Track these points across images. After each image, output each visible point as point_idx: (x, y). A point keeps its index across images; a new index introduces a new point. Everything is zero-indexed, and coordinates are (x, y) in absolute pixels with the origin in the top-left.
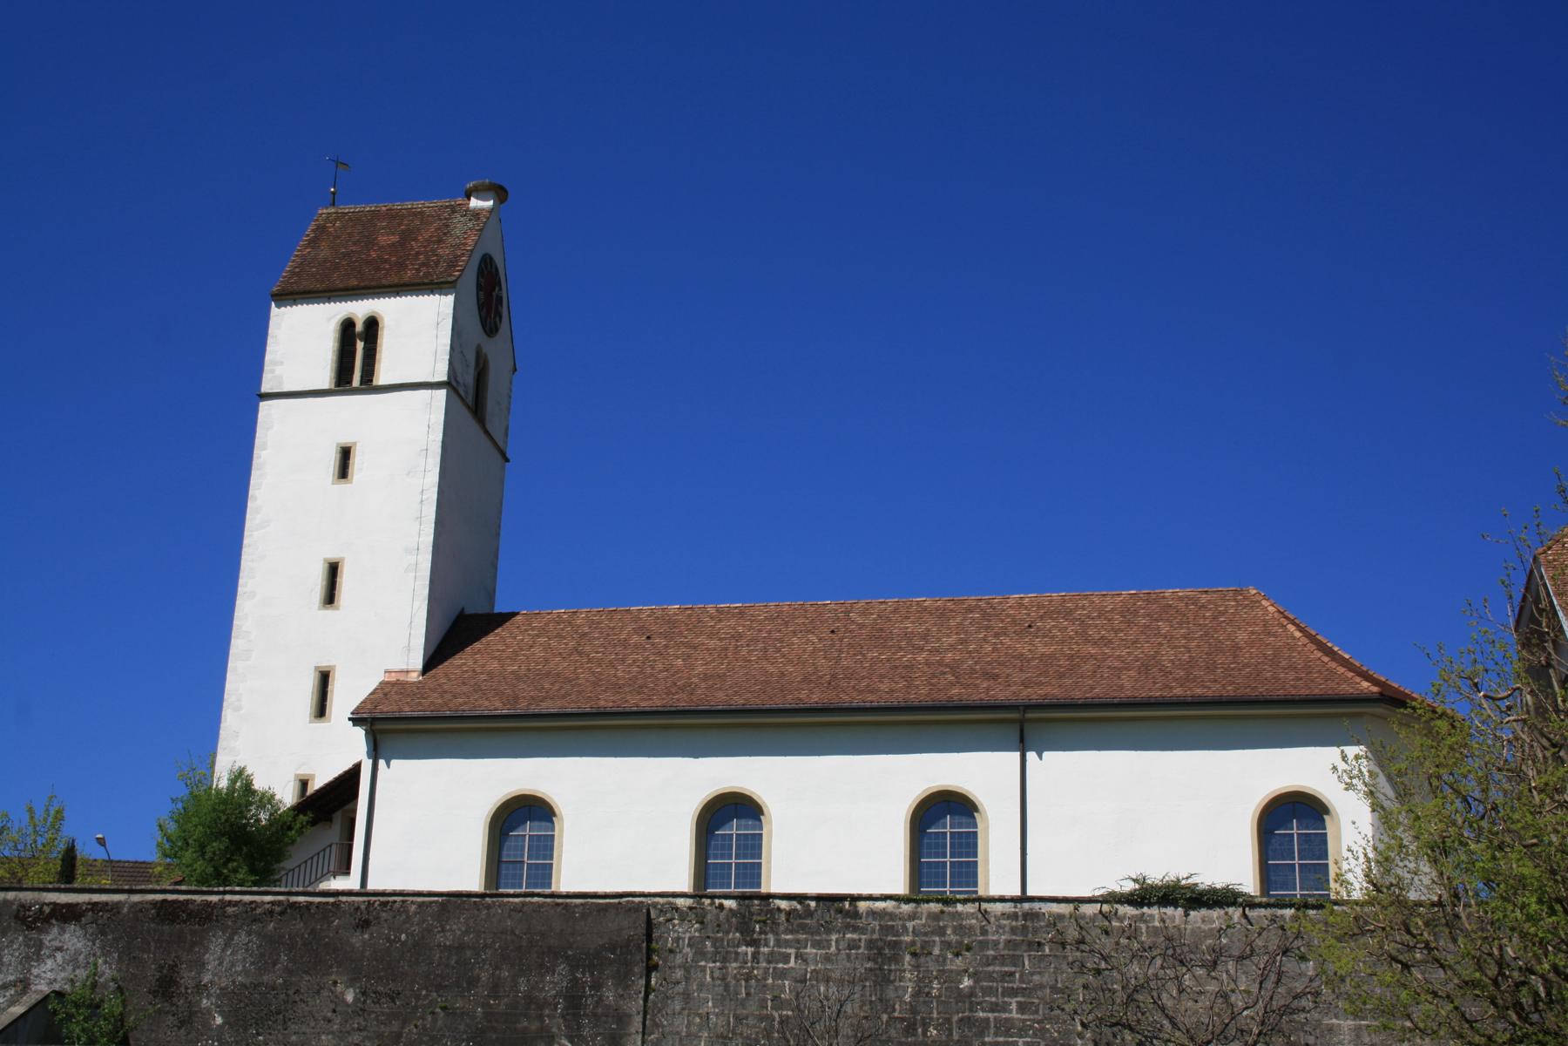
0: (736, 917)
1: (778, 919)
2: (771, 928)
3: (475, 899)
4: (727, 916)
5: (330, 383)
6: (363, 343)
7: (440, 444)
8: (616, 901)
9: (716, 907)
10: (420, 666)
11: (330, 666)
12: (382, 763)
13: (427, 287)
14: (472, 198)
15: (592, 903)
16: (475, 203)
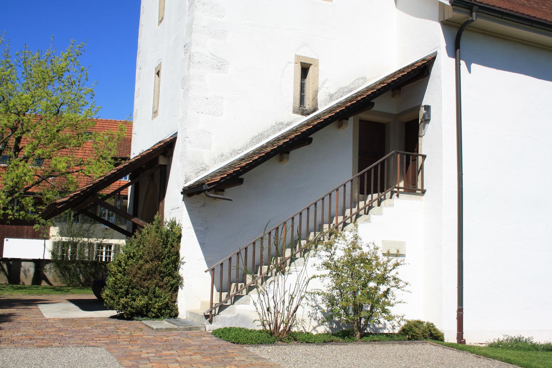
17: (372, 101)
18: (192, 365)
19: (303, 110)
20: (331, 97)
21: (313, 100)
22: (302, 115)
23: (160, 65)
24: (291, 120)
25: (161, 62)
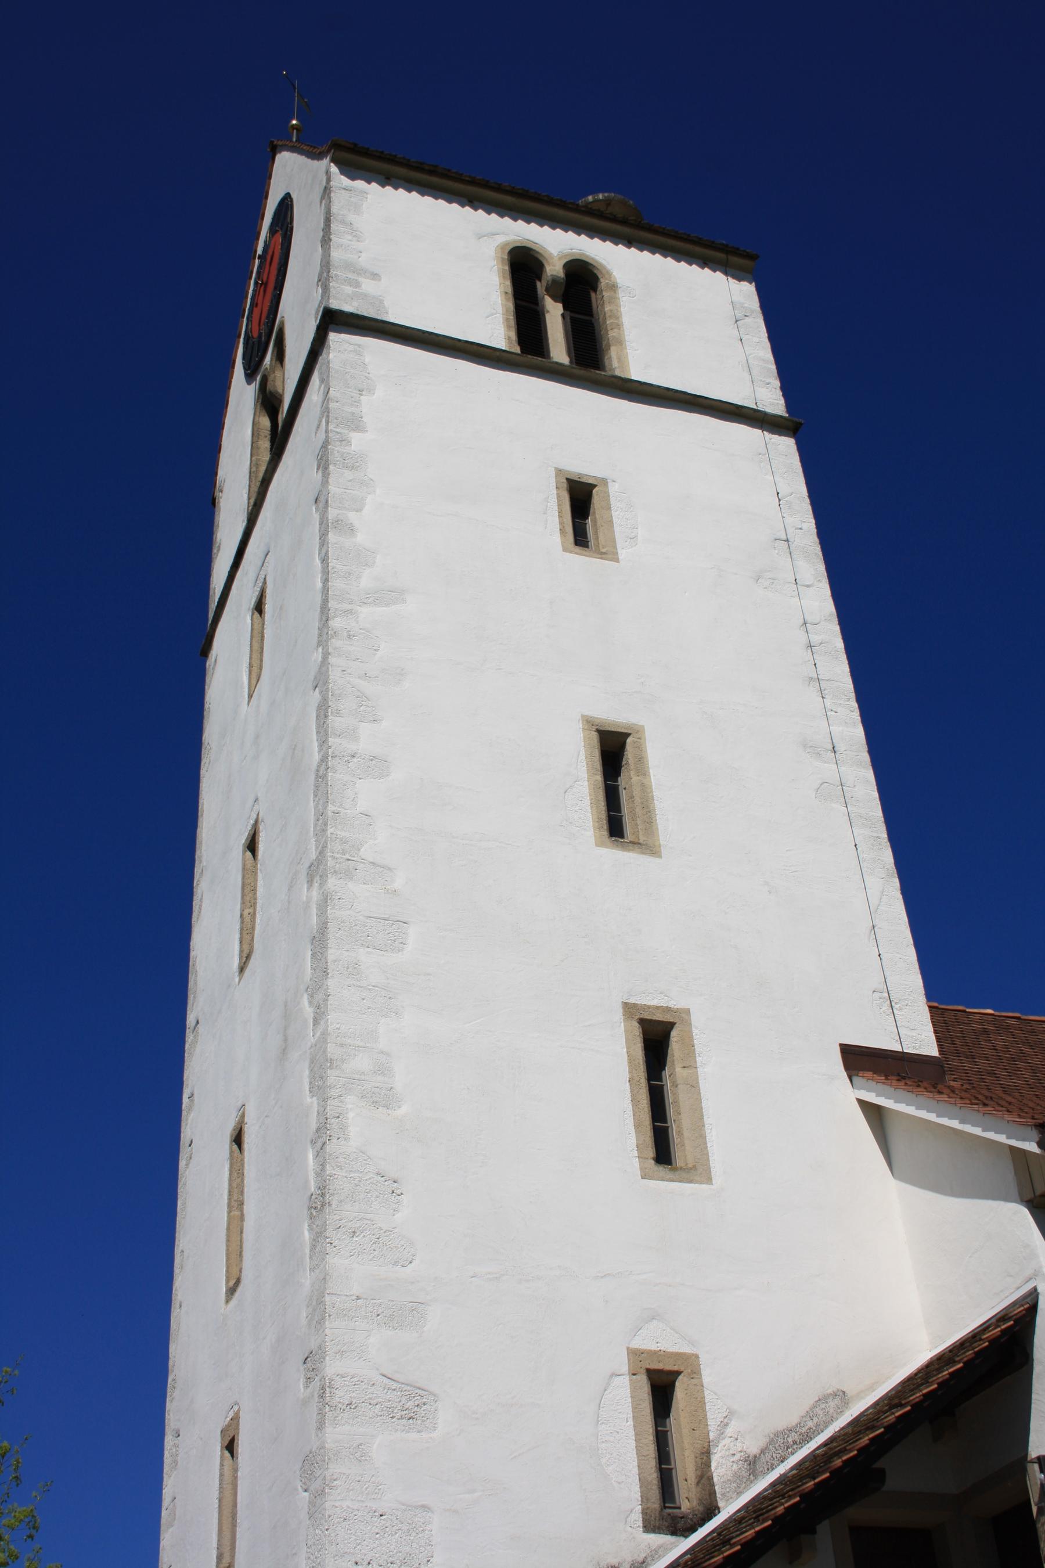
17: (877, 1465)
18: (317, 689)
19: (674, 1519)
20: (753, 1465)
21: (698, 1483)
22: (674, 1533)
23: (236, 1419)
24: (643, 1555)
25: (239, 1410)
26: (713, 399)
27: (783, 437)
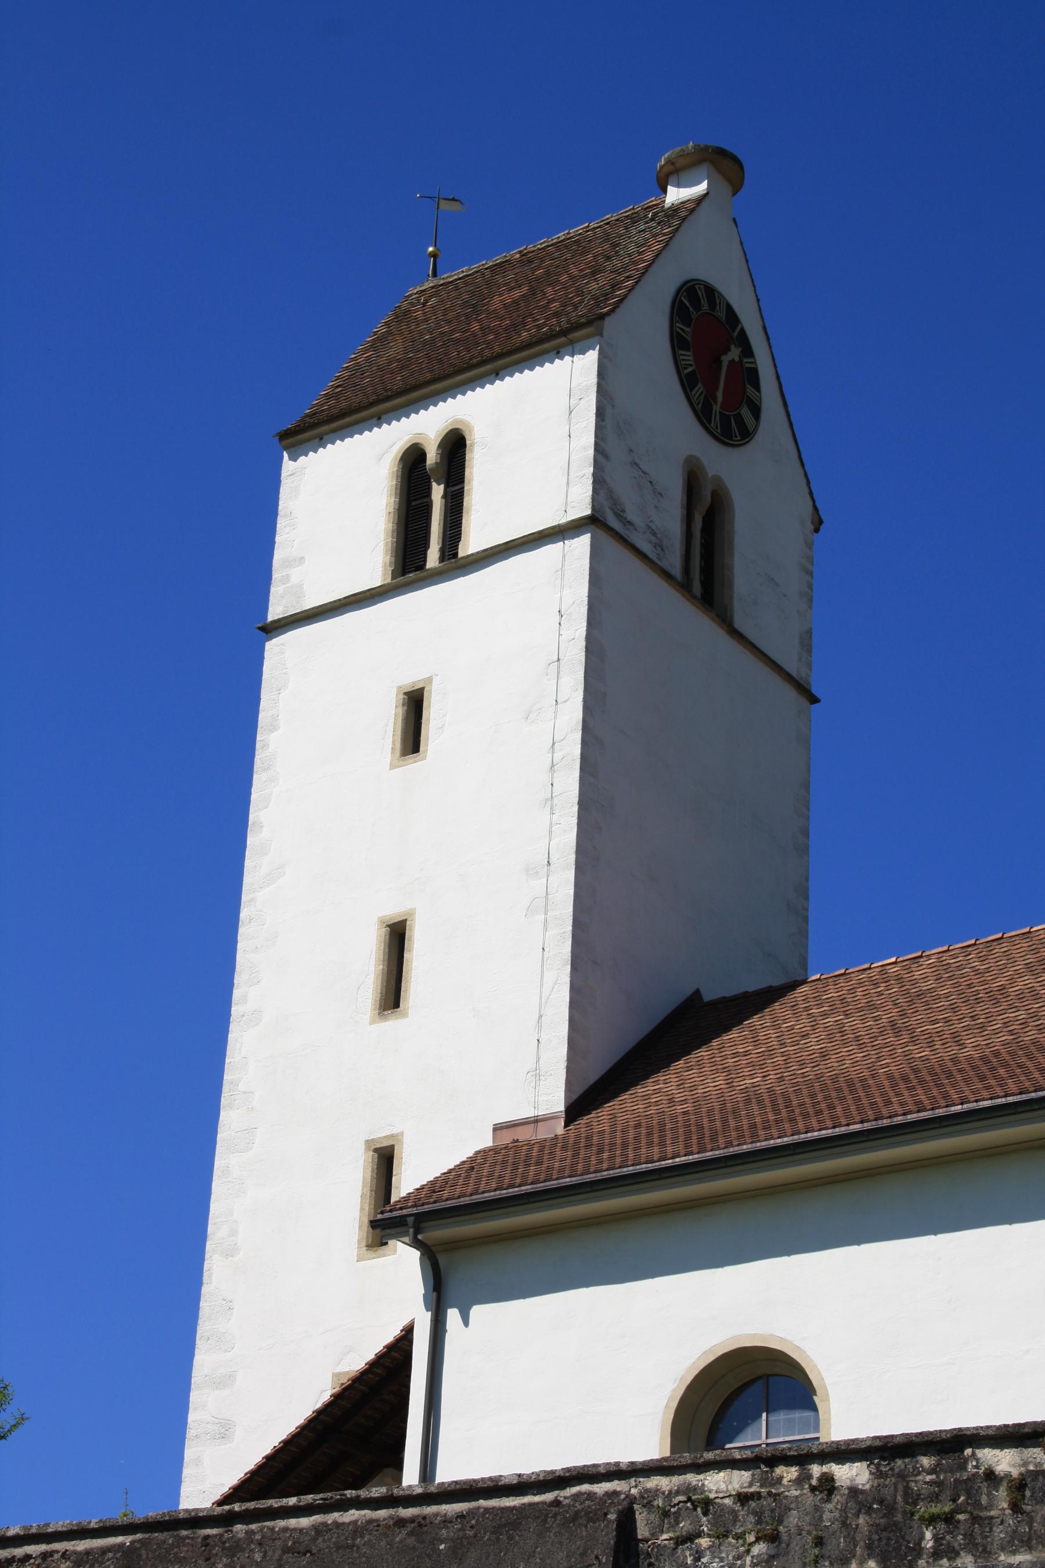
0: (869, 1510)
1: (990, 1507)
2: (969, 1536)
3: (208, 1531)
4: (844, 1510)
5: (384, 574)
6: (442, 486)
7: (584, 643)
8: (549, 1497)
9: (813, 1489)
10: (561, 1107)
11: (392, 1136)
12: (453, 1315)
13: (546, 346)
14: (669, 188)
15: (487, 1510)
16: (675, 195)
26: (376, 588)
27: (582, 537)
